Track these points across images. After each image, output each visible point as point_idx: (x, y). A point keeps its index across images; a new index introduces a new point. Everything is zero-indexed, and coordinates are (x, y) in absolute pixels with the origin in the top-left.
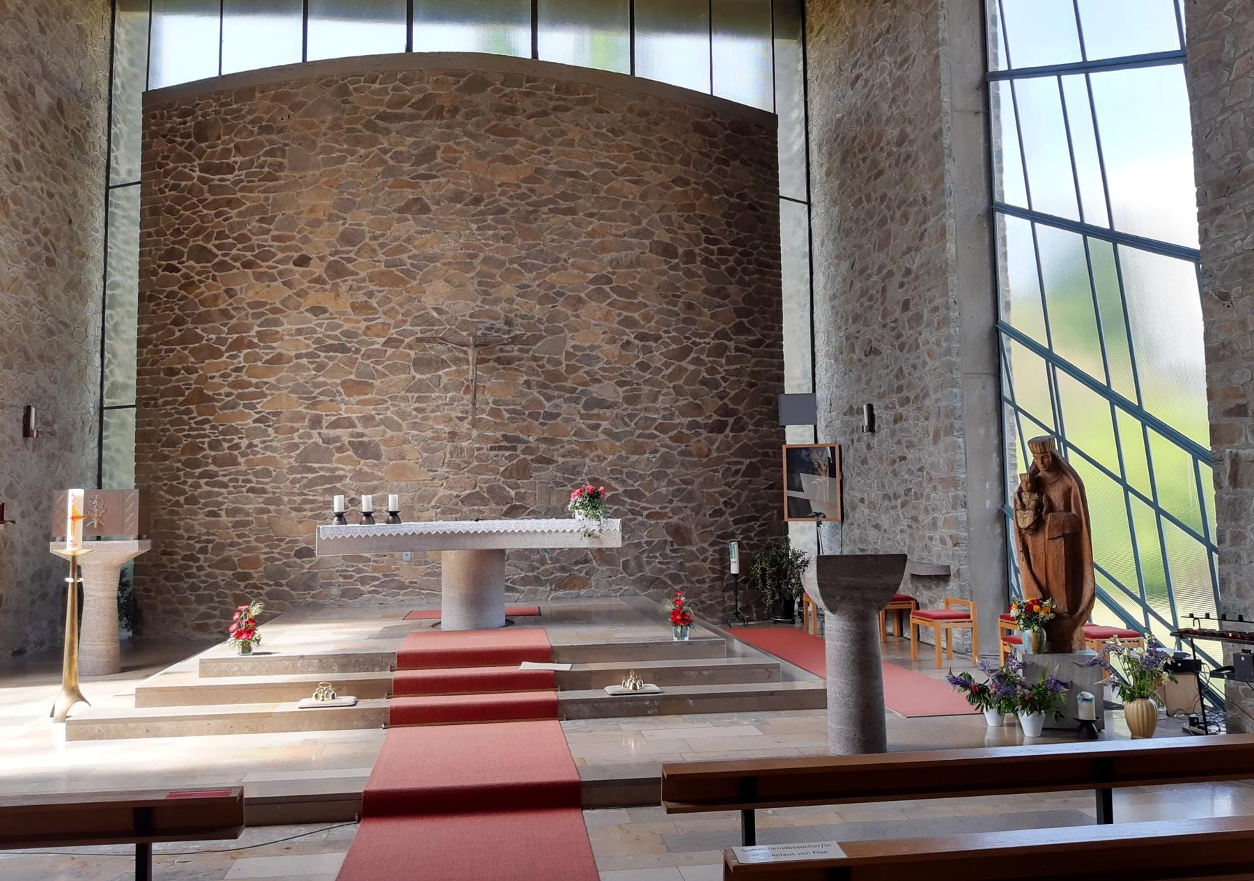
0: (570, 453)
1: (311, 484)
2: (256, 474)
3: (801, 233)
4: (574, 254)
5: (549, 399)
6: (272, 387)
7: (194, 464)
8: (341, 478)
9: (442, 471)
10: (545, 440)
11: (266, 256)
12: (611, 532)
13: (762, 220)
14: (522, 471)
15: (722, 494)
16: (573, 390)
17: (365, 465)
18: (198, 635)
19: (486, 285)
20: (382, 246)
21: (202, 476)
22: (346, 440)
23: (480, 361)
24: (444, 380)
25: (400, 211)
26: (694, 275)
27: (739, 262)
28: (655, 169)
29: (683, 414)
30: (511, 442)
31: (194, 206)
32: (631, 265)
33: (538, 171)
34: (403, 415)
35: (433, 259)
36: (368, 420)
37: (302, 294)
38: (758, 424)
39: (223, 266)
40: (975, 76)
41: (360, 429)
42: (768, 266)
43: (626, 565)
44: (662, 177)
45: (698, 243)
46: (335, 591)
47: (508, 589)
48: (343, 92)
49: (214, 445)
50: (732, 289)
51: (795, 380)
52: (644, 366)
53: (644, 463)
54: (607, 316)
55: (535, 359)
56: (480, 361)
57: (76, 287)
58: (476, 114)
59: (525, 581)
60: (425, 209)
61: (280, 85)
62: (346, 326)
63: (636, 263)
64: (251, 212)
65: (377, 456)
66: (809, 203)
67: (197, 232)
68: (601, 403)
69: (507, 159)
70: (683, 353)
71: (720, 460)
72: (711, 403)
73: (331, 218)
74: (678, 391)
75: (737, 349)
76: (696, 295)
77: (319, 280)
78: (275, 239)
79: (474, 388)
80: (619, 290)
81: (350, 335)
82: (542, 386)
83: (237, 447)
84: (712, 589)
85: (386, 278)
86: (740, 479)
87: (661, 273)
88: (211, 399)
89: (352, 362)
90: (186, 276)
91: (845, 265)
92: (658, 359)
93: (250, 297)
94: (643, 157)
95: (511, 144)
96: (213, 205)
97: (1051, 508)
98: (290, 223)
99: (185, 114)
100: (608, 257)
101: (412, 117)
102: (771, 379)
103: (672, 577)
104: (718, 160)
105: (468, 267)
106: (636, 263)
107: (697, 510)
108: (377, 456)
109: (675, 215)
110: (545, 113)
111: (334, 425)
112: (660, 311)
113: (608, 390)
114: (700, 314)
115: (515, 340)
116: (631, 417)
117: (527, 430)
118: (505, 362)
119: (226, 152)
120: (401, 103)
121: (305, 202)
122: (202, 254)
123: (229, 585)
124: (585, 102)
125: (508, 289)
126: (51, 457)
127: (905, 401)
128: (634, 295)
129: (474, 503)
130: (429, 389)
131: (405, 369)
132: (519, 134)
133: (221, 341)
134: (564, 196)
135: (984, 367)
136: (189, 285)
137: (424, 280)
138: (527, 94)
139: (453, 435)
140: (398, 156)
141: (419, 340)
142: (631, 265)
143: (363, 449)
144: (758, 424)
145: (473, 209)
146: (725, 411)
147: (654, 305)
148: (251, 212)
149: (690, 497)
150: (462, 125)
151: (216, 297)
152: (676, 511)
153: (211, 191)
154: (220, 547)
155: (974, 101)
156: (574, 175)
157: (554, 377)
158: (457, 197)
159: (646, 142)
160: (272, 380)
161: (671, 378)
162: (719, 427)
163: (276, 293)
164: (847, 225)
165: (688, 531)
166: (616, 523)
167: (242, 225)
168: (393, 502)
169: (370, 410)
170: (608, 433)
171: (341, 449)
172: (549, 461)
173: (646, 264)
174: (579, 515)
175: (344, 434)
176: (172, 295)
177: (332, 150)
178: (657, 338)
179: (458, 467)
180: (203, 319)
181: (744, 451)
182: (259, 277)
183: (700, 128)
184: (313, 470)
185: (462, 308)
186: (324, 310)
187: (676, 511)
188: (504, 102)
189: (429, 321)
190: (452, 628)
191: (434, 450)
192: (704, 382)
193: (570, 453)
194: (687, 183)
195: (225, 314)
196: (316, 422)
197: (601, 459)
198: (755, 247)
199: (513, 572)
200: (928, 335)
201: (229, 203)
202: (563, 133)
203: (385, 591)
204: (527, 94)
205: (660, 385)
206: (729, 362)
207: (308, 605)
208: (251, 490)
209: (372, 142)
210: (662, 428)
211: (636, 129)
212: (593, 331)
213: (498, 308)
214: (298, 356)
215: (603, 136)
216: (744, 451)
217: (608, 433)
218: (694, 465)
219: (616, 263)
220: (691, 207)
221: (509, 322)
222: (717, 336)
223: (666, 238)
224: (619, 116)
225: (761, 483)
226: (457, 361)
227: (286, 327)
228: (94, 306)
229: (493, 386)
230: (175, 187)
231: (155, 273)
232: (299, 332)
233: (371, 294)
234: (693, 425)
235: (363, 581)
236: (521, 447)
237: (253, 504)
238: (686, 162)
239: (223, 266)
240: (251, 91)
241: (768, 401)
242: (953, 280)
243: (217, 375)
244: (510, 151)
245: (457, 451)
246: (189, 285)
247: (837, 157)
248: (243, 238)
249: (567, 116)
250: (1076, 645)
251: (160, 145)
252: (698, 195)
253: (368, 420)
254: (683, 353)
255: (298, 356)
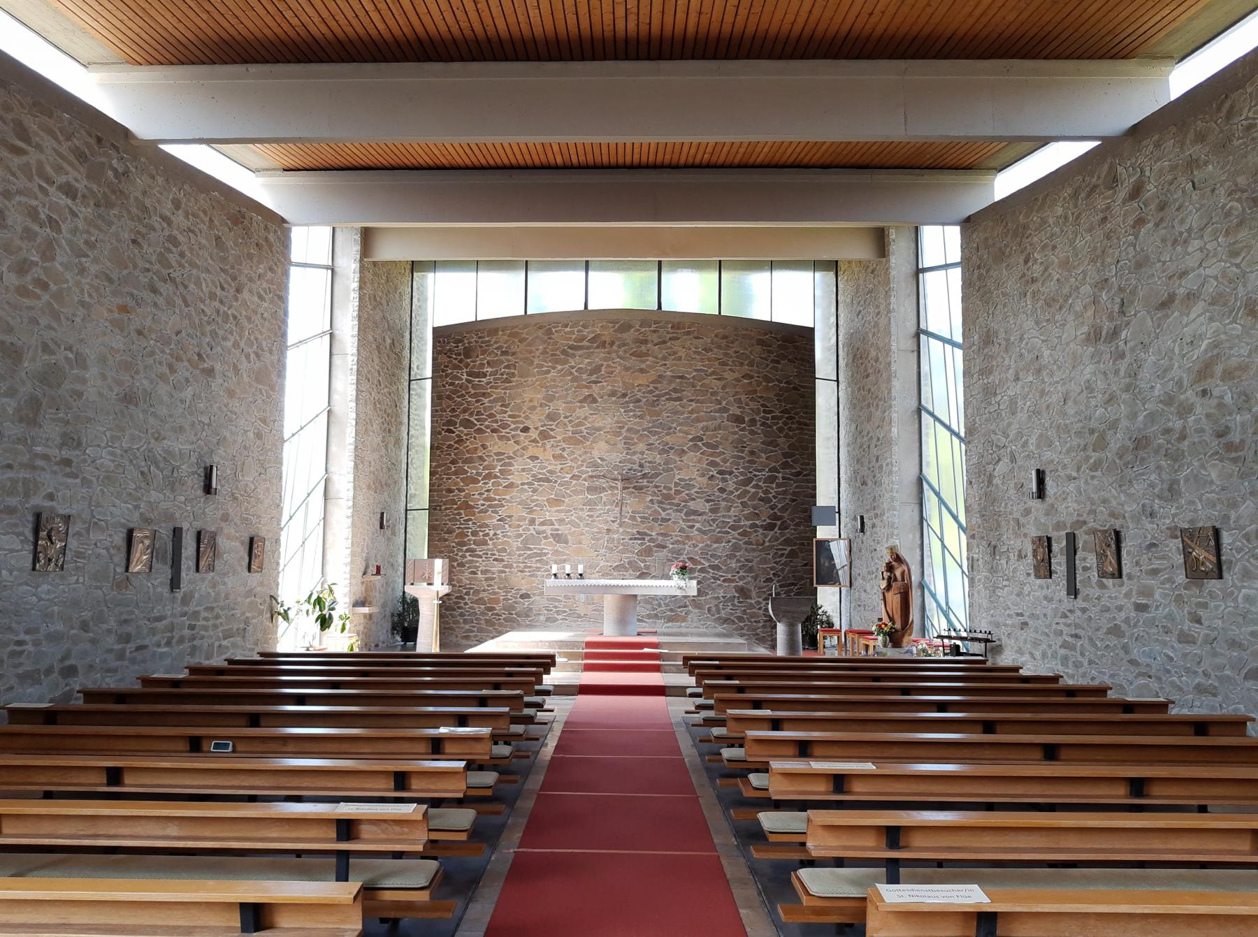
0: (677, 542)
1: (530, 557)
2: (499, 551)
3: (827, 399)
4: (681, 424)
5: (664, 510)
6: (508, 501)
7: (462, 544)
8: (546, 554)
9: (602, 551)
10: (662, 534)
11: (505, 426)
12: (692, 587)
13: (803, 396)
14: (648, 552)
15: (772, 569)
16: (678, 505)
17: (559, 547)
18: (464, 642)
19: (628, 444)
20: (570, 422)
21: (467, 551)
22: (549, 532)
23: (625, 488)
24: (604, 499)
25: (580, 402)
26: (756, 433)
27: (785, 424)
28: (731, 370)
29: (747, 519)
30: (642, 535)
31: (463, 396)
32: (715, 429)
33: (660, 376)
34: (580, 518)
35: (599, 429)
36: (561, 521)
37: (524, 448)
38: (797, 525)
39: (480, 431)
40: (913, 329)
41: (557, 527)
42: (806, 425)
43: (709, 609)
44: (736, 375)
45: (758, 414)
46: (542, 618)
47: (639, 620)
48: (549, 332)
49: (475, 534)
50: (780, 441)
51: (825, 495)
52: (722, 490)
53: (722, 549)
54: (700, 461)
55: (656, 487)
56: (625, 488)
57: (398, 442)
58: (624, 345)
59: (649, 616)
60: (595, 401)
61: (513, 328)
62: (550, 468)
63: (719, 428)
64: (495, 401)
65: (566, 542)
66: (837, 381)
67: (465, 411)
68: (695, 513)
69: (642, 371)
70: (747, 482)
71: (771, 547)
72: (765, 512)
73: (541, 405)
74: (744, 505)
75: (784, 478)
76: (757, 445)
77: (534, 441)
78: (510, 416)
79: (621, 504)
80: (707, 445)
81: (551, 472)
82: (661, 502)
83: (487, 535)
84: (764, 626)
85: (574, 440)
86: (784, 559)
87: (735, 433)
88: (473, 507)
89: (552, 488)
90: (458, 436)
91: (854, 426)
92: (731, 485)
93: (495, 449)
94: (724, 364)
95: (644, 362)
96: (474, 396)
97: (896, 580)
98: (519, 408)
99: (460, 341)
100: (701, 425)
101: (588, 348)
102: (806, 496)
103: (738, 618)
104: (773, 361)
105: (619, 434)
106: (719, 428)
107: (755, 578)
108: (566, 542)
109: (743, 397)
110: (665, 342)
111: (542, 524)
112: (733, 457)
113: (700, 505)
114: (759, 457)
115: (644, 476)
116: (714, 521)
117: (651, 529)
118: (639, 489)
119: (482, 365)
120: (582, 340)
121: (527, 395)
122: (467, 424)
123: (483, 614)
124: (688, 333)
125: (641, 446)
126: (389, 539)
127: (876, 516)
128: (716, 447)
129: (620, 570)
130: (595, 504)
131: (582, 492)
132: (648, 355)
133: (479, 474)
134: (675, 390)
135: (913, 499)
136: (460, 441)
137: (594, 442)
138: (654, 331)
139: (608, 530)
140: (579, 370)
141: (591, 477)
142: (715, 429)
143: (558, 538)
144: (797, 525)
145: (623, 400)
146: (775, 517)
147: (729, 453)
148: (495, 401)
149: (751, 570)
150: (617, 352)
151: (476, 449)
152: (742, 578)
153: (474, 387)
154: (477, 592)
155: (911, 344)
156: (681, 377)
157: (668, 497)
158: (613, 394)
159: (726, 355)
160: (507, 497)
161: (739, 497)
162: (770, 527)
163: (510, 448)
164: (855, 401)
165: (750, 591)
166: (694, 582)
167: (491, 408)
168: (580, 569)
169: (562, 515)
170: (699, 530)
171: (546, 538)
172: (664, 547)
173: (725, 428)
174: (676, 577)
175: (548, 529)
176: (450, 446)
177: (543, 366)
178: (731, 473)
179: (611, 549)
180: (467, 461)
181: (787, 542)
182: (501, 438)
183: (761, 343)
184: (530, 549)
185: (615, 457)
186: (537, 458)
187: (742, 578)
188: (641, 337)
189: (596, 466)
190: (609, 632)
191: (598, 539)
192: (761, 499)
193: (677, 542)
194: (752, 377)
195: (481, 458)
196: (532, 522)
197: (695, 546)
198: (797, 414)
199: (642, 610)
200: (885, 480)
201: (484, 395)
202: (675, 353)
203: (570, 619)
204: (654, 331)
205: (733, 501)
206: (778, 486)
207: (527, 626)
208: (496, 560)
209: (566, 362)
210: (733, 528)
211: (719, 347)
212: (691, 469)
213: (634, 458)
214: (523, 484)
215: (699, 353)
216: (787, 542)
217: (699, 530)
218: (754, 550)
219: (706, 429)
220: (755, 392)
221: (641, 466)
222: (770, 471)
223: (738, 412)
224: (709, 340)
225: (798, 562)
226: (612, 488)
227: (516, 467)
228: (404, 451)
229: (632, 503)
230: (451, 384)
231: (440, 433)
232: (523, 470)
233: (563, 450)
234: (753, 526)
235: (558, 613)
236: (647, 538)
237: (497, 567)
238: (751, 364)
239: (480, 431)
240: (496, 330)
241: (805, 511)
242: (895, 448)
243: (476, 493)
244: (643, 366)
245: (611, 540)
246: (460, 441)
247: (851, 356)
248: (491, 416)
249: (677, 343)
250: (904, 644)
251: (443, 359)
252: (759, 384)
253: (561, 521)
254: (747, 482)
255: (523, 484)
